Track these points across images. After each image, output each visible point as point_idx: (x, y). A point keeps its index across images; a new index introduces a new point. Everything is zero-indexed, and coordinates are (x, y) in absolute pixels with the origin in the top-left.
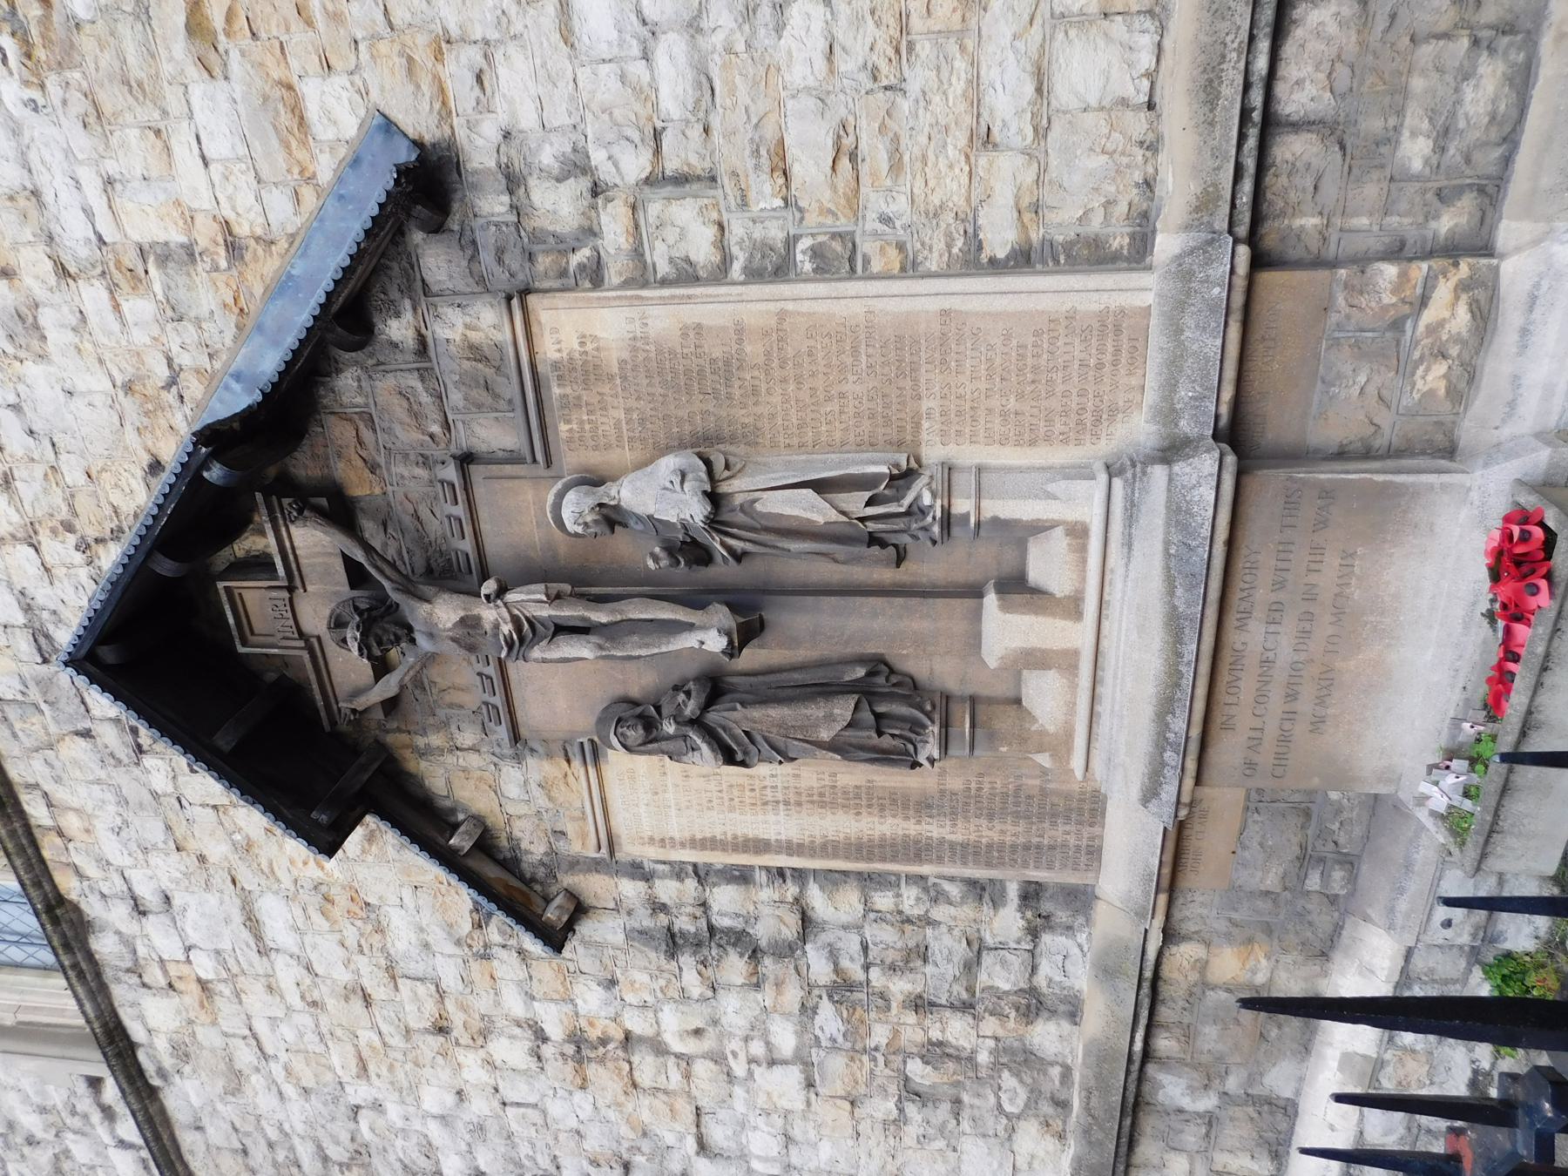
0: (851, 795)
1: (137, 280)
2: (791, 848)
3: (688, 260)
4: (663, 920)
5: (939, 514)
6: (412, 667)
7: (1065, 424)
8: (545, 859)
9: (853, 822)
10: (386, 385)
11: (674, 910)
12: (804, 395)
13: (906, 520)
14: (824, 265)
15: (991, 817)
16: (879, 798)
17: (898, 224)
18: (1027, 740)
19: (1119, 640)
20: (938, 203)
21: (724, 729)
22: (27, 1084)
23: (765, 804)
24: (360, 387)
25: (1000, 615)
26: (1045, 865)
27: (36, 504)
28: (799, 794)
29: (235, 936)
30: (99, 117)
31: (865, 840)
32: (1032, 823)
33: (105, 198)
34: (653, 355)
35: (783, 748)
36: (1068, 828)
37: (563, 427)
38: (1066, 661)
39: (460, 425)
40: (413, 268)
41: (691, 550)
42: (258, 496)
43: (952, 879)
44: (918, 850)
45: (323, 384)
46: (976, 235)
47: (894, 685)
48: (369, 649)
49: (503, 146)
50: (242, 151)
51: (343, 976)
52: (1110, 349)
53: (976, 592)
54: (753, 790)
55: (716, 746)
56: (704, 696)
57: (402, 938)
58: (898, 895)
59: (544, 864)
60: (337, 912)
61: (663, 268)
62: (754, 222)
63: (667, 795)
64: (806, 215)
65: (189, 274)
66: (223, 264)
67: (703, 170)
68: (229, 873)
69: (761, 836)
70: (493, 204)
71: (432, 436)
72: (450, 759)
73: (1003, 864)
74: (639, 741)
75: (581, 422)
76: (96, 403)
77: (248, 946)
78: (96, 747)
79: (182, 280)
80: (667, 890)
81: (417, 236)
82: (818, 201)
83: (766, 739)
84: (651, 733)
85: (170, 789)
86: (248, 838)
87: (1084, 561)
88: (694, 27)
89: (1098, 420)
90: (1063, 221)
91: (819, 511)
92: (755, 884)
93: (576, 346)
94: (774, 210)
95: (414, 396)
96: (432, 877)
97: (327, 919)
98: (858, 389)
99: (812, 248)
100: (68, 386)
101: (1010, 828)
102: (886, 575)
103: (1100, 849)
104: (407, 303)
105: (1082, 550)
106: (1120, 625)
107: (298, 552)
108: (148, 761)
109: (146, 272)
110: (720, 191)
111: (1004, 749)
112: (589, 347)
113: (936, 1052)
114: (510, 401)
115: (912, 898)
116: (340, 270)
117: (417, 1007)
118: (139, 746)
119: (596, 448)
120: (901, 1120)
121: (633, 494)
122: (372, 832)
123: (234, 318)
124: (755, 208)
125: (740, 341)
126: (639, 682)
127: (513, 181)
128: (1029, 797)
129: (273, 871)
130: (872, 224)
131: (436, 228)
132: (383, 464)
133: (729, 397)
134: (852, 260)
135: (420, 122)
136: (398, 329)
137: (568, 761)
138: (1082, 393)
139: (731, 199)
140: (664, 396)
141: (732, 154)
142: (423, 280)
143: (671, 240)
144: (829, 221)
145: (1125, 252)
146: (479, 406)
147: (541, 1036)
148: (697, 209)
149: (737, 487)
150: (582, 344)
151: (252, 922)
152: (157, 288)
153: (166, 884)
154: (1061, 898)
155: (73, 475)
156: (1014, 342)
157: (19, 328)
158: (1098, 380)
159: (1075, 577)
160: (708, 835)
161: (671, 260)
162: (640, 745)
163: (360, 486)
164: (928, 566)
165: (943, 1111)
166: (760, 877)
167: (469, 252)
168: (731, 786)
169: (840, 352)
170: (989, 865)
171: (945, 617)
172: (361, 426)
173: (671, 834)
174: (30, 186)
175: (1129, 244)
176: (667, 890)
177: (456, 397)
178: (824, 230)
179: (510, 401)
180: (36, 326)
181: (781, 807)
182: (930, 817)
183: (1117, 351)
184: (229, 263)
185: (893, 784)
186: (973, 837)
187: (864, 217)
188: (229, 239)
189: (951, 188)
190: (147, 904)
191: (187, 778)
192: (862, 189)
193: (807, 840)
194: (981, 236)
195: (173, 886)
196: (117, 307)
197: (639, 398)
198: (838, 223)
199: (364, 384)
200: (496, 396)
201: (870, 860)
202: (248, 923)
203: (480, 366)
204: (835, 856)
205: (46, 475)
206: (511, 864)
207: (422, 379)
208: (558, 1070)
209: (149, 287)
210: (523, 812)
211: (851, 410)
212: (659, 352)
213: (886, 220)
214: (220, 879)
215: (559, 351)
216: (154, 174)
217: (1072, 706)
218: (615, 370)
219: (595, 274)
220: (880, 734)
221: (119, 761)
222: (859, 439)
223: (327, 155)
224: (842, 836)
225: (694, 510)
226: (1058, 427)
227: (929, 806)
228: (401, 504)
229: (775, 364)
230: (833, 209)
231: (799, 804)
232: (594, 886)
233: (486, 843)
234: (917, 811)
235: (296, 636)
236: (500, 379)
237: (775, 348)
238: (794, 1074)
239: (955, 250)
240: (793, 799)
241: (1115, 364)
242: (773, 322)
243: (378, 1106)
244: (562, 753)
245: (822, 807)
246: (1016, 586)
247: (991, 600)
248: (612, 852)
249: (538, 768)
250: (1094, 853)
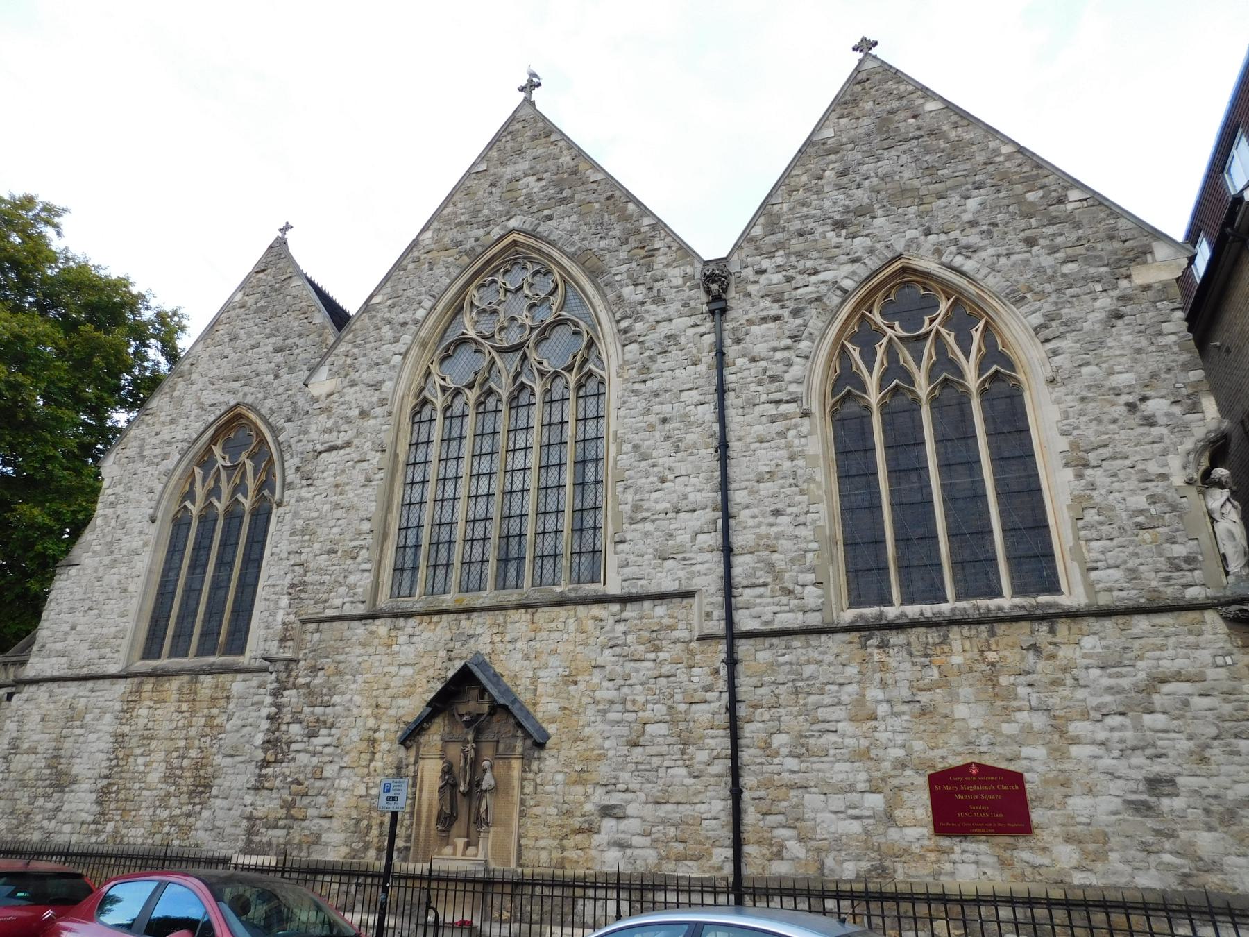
1: (532, 683)
14: (522, 812)
18: (441, 846)
22: (362, 583)
29: (402, 659)
38: (454, 854)
41: (479, 784)
44: (418, 825)
51: (392, 685)
57: (402, 702)
70: (536, 755)
80: (411, 768)
88: (556, 793)
90: (525, 852)
102: (472, 819)
113: (369, 827)
117: (382, 701)
120: (351, 819)
121: (488, 775)
126: (456, 769)
127: (539, 758)
135: (549, 743)
141: (538, 797)
147: (375, 731)
149: (488, 795)
151: (406, 665)
155: (502, 657)
163: (495, 718)
164: (473, 828)
165: (352, 829)
171: (464, 832)
176: (411, 768)
189: (530, 834)
206: (419, 734)
208: (366, 734)
214: (417, 660)
219: (524, 771)
225: (484, 787)
232: (413, 752)
233: (423, 729)
238: (363, 792)
243: (355, 682)
246: (468, 845)
249: (439, 744)
250: (416, 861)
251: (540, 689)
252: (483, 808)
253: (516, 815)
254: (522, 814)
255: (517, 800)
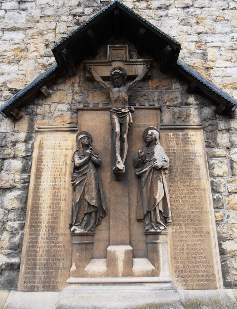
0: (57, 205)
1: (199, 47)
2: (37, 186)
3: (214, 168)
4: (9, 144)
5: (158, 231)
6: (105, 85)
7: (181, 267)
8: (34, 113)
9: (47, 206)
10: (179, 95)
11: (13, 148)
12: (184, 195)
13: (155, 222)
14: (216, 201)
15: (47, 251)
16: (56, 214)
17: (228, 220)
19: (120, 290)
20: (233, 230)
21: (88, 167)
23: (55, 178)
24: (177, 89)
25: (124, 251)
26: (27, 271)
27: (143, 12)
28: (58, 189)
30: (232, 49)
31: (40, 209)
32: (45, 266)
33: (216, 46)
34: (191, 157)
35: (81, 184)
36: (42, 278)
37: (171, 134)
39: (169, 110)
40: (206, 105)
42: (152, 59)
43: (22, 239)
44: (35, 227)
45: (177, 81)
46: (227, 240)
47: (99, 219)
48: (116, 75)
49: (235, 129)
50: (228, 75)
52: (203, 278)
53: (130, 244)
54: (60, 175)
55: (82, 164)
56: (97, 162)
58: (14, 220)
59: (32, 112)
60: (17, 52)
61: (212, 162)
62: (224, 184)
63: (58, 149)
64: (227, 197)
65: (200, 58)
66: (204, 66)
67: (235, 173)
68: (32, 27)
69: (42, 177)
71: (166, 103)
72: (70, 92)
73: (28, 256)
74: (83, 142)
75: (173, 138)
76: (169, 31)
77: (6, 26)
78: (75, 6)
79: (199, 56)
80: (21, 148)
81: (214, 108)
82: (232, 200)
83: (84, 179)
84: (85, 146)
85: (61, 20)
86: (45, 35)
87: (144, 276)
89: (182, 276)
91: (159, 197)
92: (21, 174)
93: (192, 140)
94: (228, 189)
95: (176, 100)
96: (29, 80)
97: (15, 49)
98: (186, 209)
99: (220, 198)
100: (172, 27)
101: (43, 258)
103: (33, 291)
104: (198, 103)
105: (148, 275)
106: (126, 290)
107: (136, 65)
108: (71, 18)
109: (200, 50)
110: (230, 177)
111: (78, 254)
112: (192, 143)
114: (175, 122)
115: (13, 225)
116: (211, 88)
118: (76, 16)
119: (166, 141)
122: (46, 67)
123: (192, 65)
124: (228, 185)
125: (197, 179)
127: (228, 130)
128: (55, 264)
129: (32, 38)
130: (227, 213)
131: (216, 112)
132: (157, 90)
133: (182, 176)
134: (218, 208)
136: (192, 100)
137: (69, 123)
138: (190, 271)
139: (229, 179)
140: (181, 159)
142: (204, 107)
143: (218, 164)
144: (227, 203)
145: (226, 281)
146: (174, 115)
148: (226, 171)
149: (164, 177)
150: (193, 141)
152: (197, 51)
153: (29, 11)
154: (10, 278)
156: (202, 251)
157: (186, 21)
158: (194, 276)
159: (139, 273)
160: (43, 161)
161: (213, 164)
162: (82, 142)
166: (25, 176)
167: (211, 118)
168: (61, 169)
169: (195, 205)
170: (28, 251)
172: (167, 87)
173: (44, 149)
174: (216, 33)
175: (229, 282)
176: (21, 148)
177: (176, 110)
178: (224, 202)
179: (175, 122)
180: (186, 25)
181: (54, 183)
182: (48, 231)
183: (203, 281)
184: (204, 67)
185: (61, 218)
186: (40, 245)
187: (228, 211)
188: (209, 68)
190: (22, 5)
191: (65, 25)
192: (234, 211)
193: (40, 191)
194: (227, 241)
195: (29, 12)
196: (192, 42)
197: (180, 153)
198: (226, 205)
199: (178, 90)
200: (176, 119)
201: (32, 211)
202: (14, 28)
203: (185, 117)
204: (33, 199)
205: (151, 16)
207: (180, 103)
209: (197, 49)
210: (52, 108)
211: (181, 207)
212: (192, 159)
213: (228, 217)
215: (191, 135)
216: (222, 57)
217: (94, 276)
218: (187, 148)
220: (85, 214)
221: (71, 10)
222: (173, 209)
223: (230, 92)
224: (42, 202)
226: (180, 265)
227: (52, 230)
228: (147, 93)
229: (192, 188)
230: (230, 204)
231: (54, 189)
232: (23, 125)
234: (51, 226)
235: (112, 60)
236: (181, 120)
237: (196, 188)
239: (223, 234)
240: (57, 187)
241: (199, 280)
242: (202, 188)
244: (72, 122)
245: (53, 196)
247: (129, 248)
248: (37, 131)
250: (32, 289)
251: (212, 53)
252: (159, 197)
253: (210, 206)
254: (218, 205)
255: (206, 183)
